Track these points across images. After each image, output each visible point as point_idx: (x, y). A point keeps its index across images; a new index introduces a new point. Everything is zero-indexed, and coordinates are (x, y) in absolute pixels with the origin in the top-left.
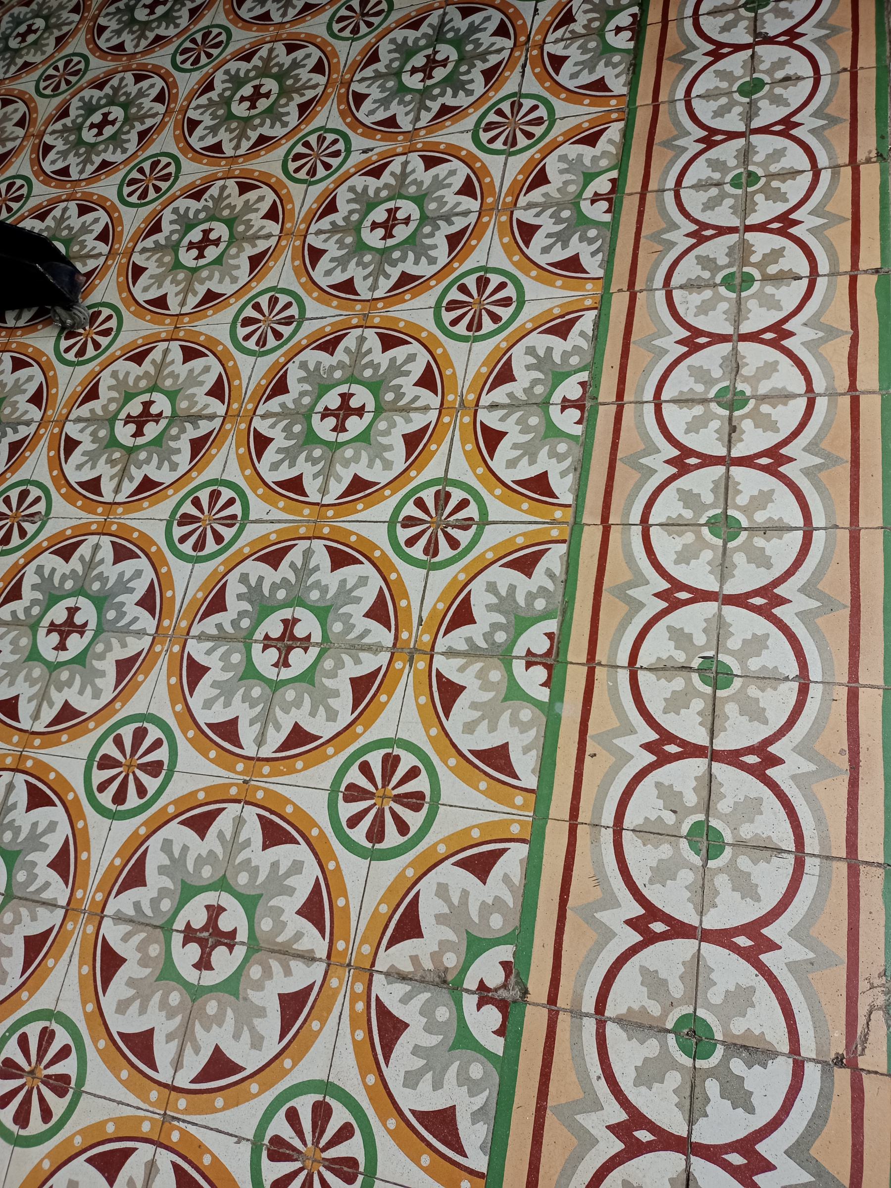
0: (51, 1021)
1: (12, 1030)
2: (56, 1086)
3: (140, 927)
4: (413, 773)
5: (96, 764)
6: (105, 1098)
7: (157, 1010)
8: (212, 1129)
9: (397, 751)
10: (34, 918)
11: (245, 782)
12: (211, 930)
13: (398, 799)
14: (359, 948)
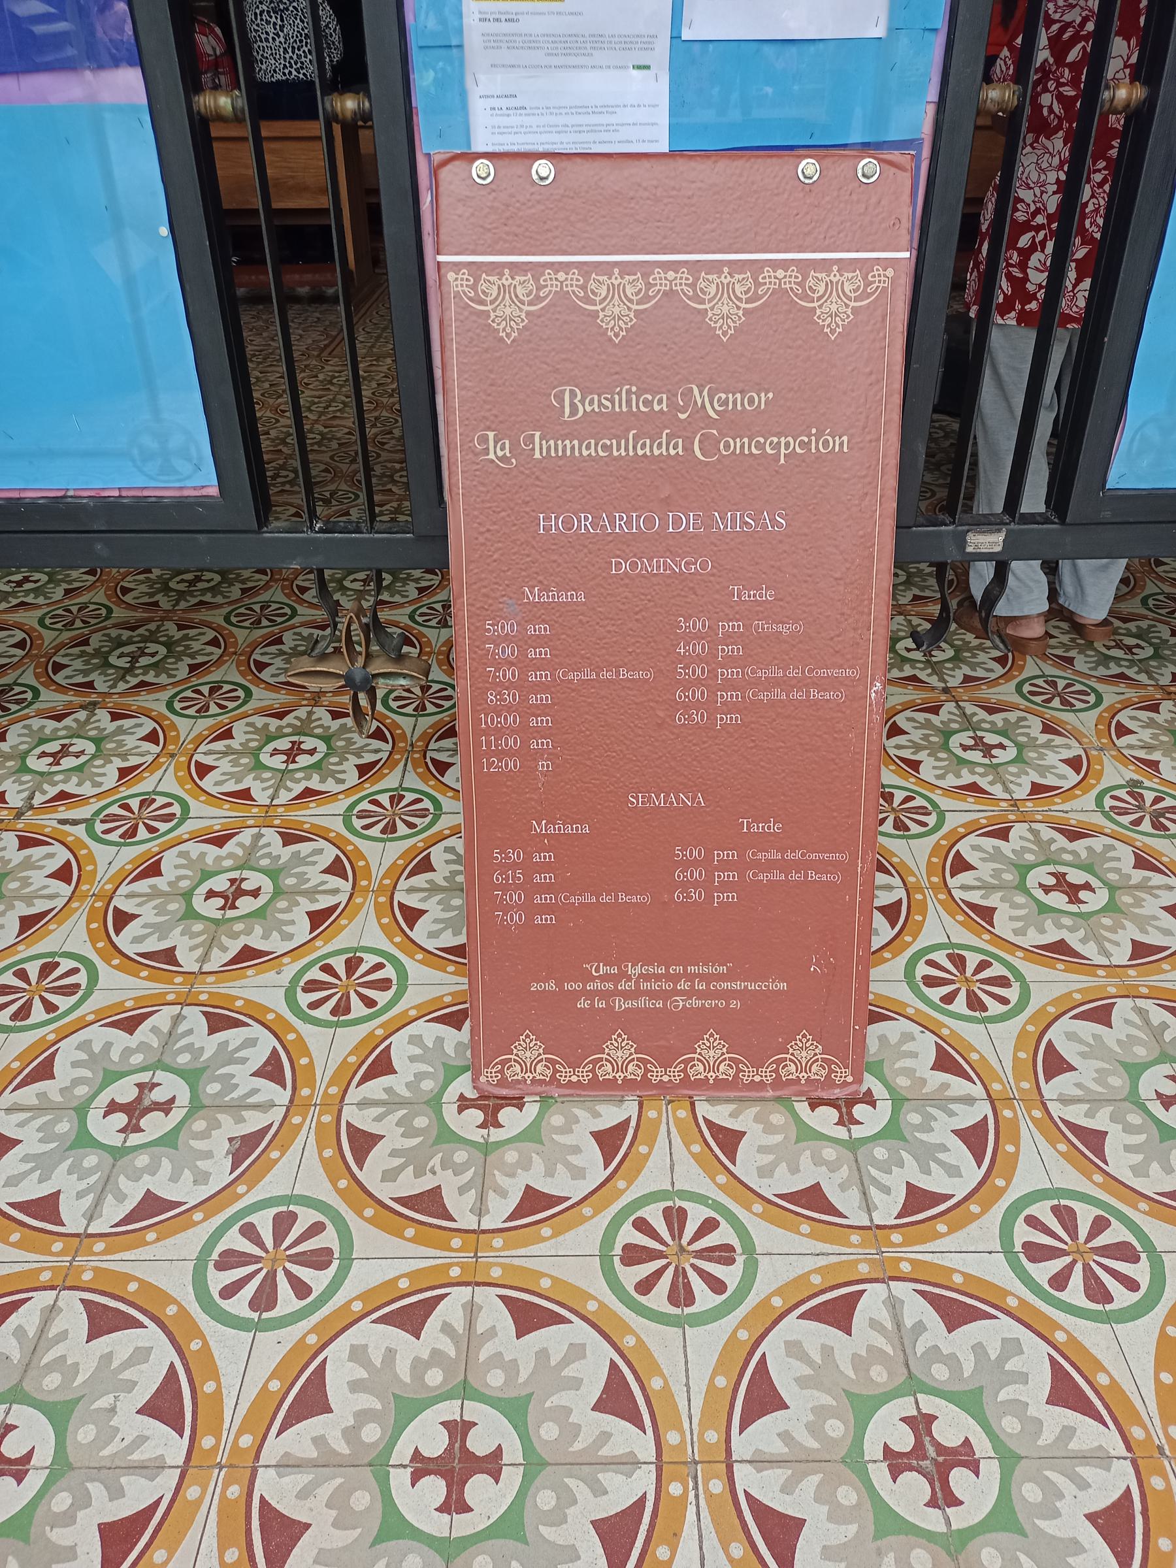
0: (743, 1253)
1: (717, 1206)
2: (677, 1287)
3: (896, 1341)
4: (717, 1286)
5: (1055, 1202)
6: (686, 1363)
7: (811, 1406)
8: (701, 1548)
9: (740, 1260)
10: (843, 1187)
11: (1160, 1449)
12: (941, 1459)
13: (680, 1273)
14: (496, 1264)
